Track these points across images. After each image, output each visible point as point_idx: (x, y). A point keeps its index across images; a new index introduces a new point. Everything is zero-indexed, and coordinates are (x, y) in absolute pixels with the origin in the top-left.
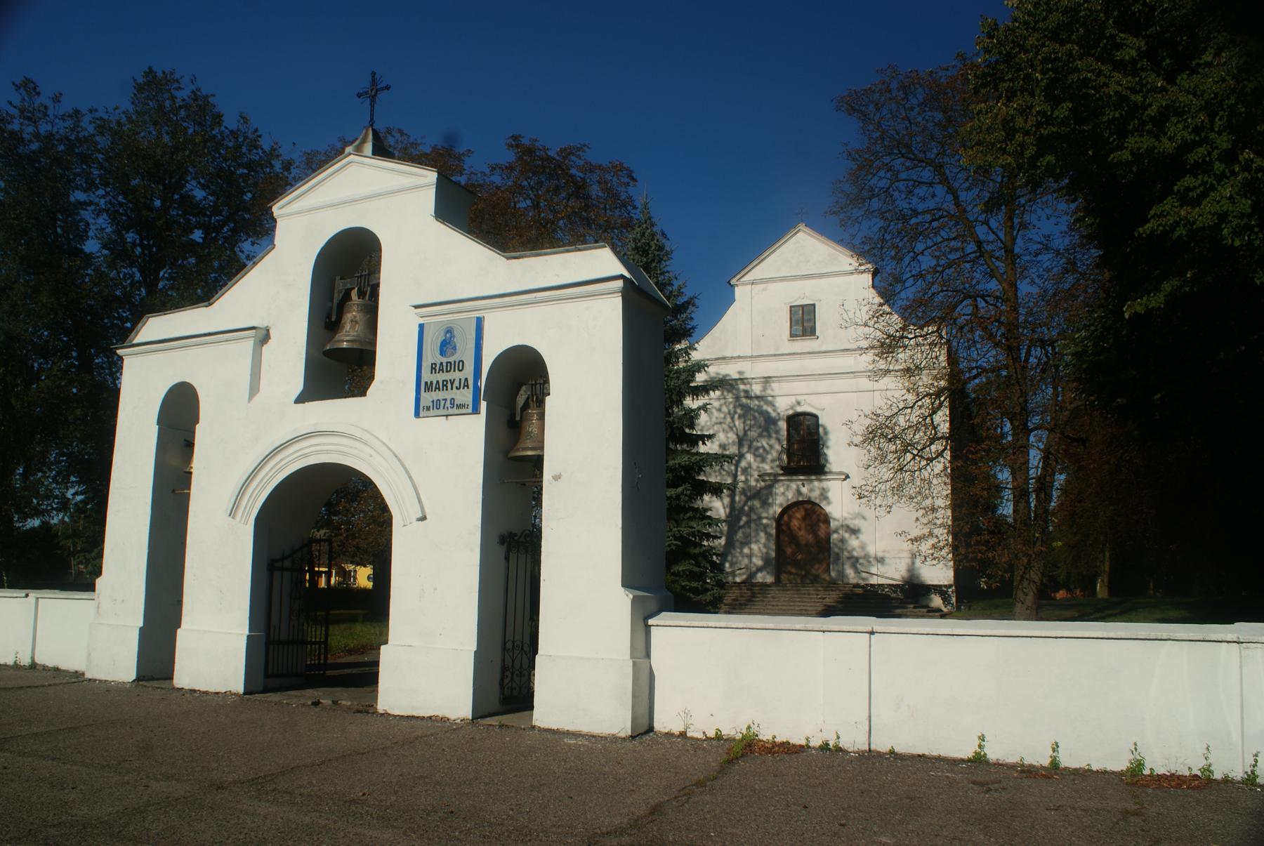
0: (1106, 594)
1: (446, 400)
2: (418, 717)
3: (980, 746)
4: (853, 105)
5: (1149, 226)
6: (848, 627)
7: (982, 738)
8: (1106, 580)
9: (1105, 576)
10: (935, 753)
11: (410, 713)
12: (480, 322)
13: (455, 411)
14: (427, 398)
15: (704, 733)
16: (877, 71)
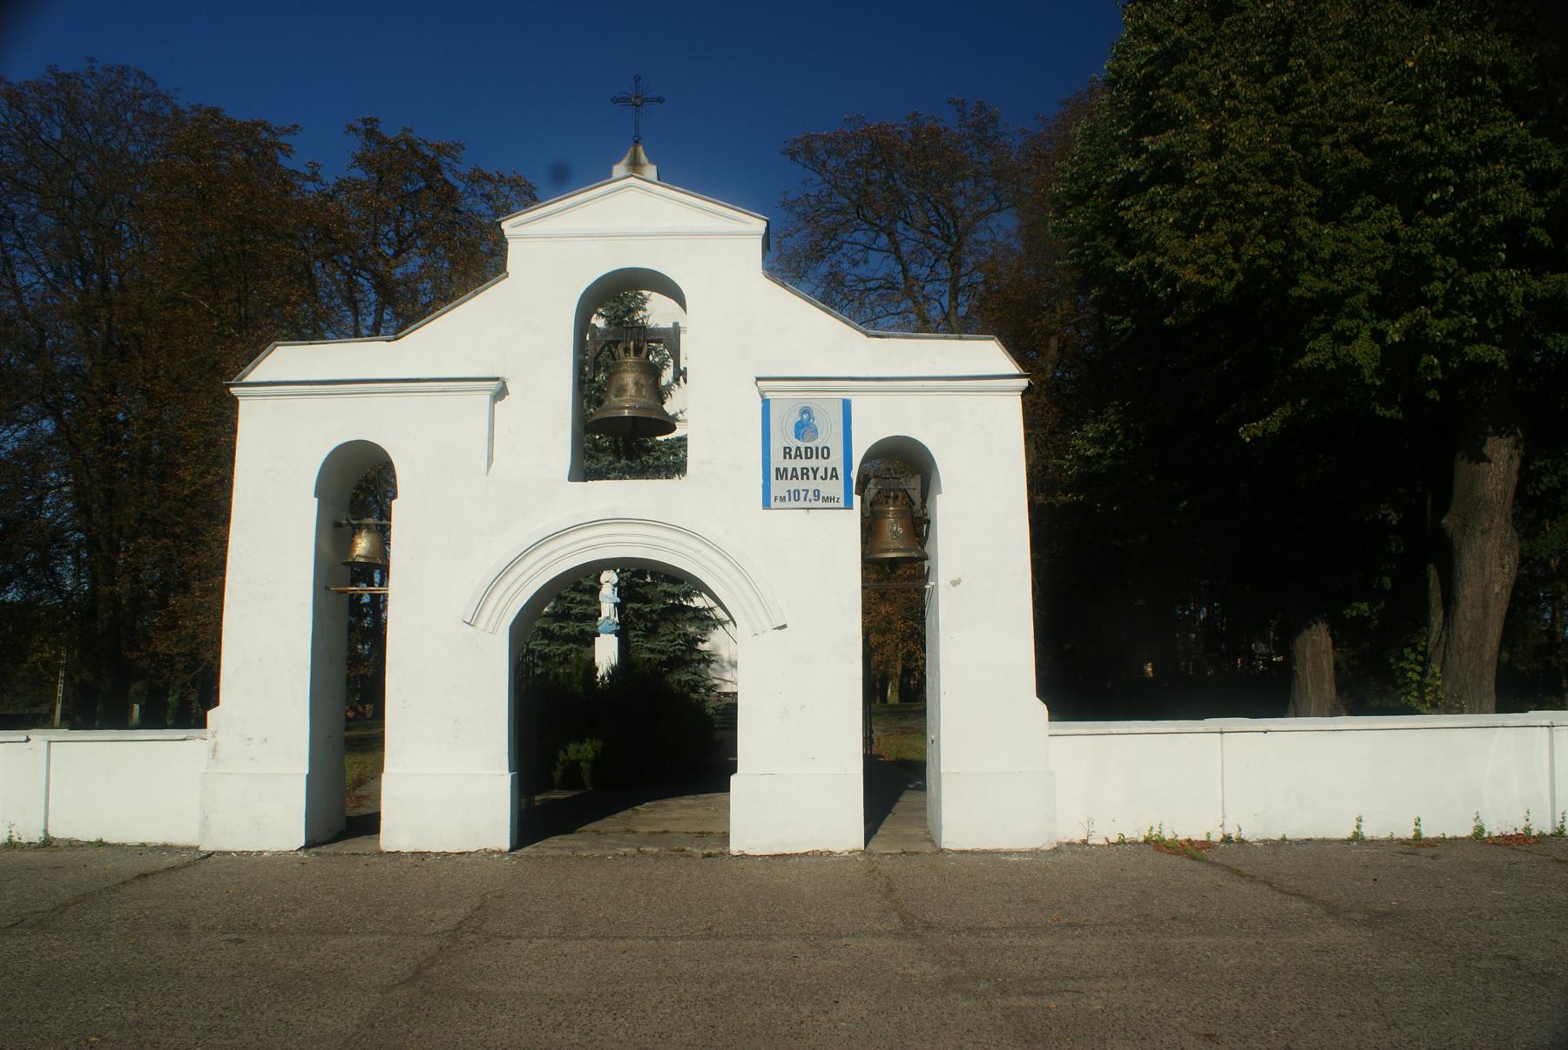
0: (897, 699)
1: (807, 491)
2: (790, 855)
3: (1358, 827)
4: (805, 151)
5: (1307, 359)
6: (1495, 722)
7: (1359, 820)
8: (897, 684)
9: (897, 680)
10: (1320, 836)
11: (778, 851)
12: (847, 406)
13: (820, 504)
14: (778, 487)
15: (1107, 839)
16: (845, 119)
